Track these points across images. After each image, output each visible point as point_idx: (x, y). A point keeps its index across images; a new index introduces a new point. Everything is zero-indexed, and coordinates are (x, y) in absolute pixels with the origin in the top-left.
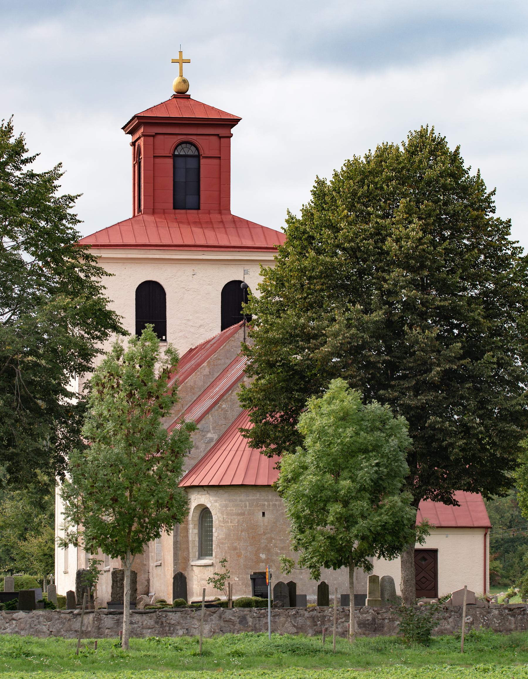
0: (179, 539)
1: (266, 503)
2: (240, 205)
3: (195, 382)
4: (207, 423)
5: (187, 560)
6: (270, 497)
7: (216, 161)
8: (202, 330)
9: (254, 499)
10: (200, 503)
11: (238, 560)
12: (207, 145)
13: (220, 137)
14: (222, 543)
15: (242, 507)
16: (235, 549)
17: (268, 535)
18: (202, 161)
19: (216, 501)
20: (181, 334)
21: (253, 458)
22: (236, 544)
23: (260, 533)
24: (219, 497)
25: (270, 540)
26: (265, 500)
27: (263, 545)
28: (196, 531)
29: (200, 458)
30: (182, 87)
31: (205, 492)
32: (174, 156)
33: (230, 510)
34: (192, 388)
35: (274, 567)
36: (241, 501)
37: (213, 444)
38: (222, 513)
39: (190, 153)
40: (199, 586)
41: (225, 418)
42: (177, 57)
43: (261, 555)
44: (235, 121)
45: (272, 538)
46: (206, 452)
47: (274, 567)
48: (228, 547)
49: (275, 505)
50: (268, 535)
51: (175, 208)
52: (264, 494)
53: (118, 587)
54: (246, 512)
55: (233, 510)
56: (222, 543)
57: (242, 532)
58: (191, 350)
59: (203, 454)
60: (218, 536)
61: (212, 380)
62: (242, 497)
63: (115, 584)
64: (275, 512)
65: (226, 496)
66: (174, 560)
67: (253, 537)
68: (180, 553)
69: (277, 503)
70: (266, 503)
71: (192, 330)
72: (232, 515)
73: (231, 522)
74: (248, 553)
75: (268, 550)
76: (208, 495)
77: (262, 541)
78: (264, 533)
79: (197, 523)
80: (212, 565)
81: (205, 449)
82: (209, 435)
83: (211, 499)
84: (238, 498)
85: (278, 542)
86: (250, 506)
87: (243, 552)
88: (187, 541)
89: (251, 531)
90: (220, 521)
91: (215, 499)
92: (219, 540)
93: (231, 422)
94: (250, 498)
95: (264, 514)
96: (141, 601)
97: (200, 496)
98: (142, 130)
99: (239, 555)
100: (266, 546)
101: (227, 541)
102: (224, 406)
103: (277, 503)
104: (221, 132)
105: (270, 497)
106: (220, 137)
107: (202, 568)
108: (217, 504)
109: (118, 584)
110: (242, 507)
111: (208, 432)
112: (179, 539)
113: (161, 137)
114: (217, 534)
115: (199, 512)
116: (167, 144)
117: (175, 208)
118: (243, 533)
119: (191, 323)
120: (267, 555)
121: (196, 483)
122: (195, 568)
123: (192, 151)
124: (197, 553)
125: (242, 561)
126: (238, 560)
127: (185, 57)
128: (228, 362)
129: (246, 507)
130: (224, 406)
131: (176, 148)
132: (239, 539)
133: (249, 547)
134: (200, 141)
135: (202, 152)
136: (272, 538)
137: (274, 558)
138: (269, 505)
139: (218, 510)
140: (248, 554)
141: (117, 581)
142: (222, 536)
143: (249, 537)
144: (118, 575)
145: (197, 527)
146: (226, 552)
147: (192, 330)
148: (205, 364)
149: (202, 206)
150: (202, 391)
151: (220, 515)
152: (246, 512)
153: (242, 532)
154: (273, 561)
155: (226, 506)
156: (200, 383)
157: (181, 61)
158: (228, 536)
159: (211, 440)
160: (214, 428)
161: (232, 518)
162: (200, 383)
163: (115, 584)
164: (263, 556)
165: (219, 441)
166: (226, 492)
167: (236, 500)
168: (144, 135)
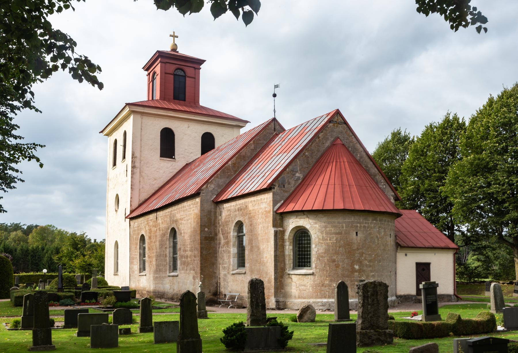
0: (278, 253)
1: (359, 225)
2: (204, 101)
3: (246, 153)
4: (296, 165)
5: (283, 269)
6: (361, 221)
7: (193, 80)
8: (192, 155)
9: (349, 222)
10: (298, 225)
11: (336, 270)
12: (189, 71)
13: (195, 68)
14: (322, 257)
15: (339, 228)
16: (334, 261)
17: (360, 251)
18: (187, 79)
19: (316, 223)
20: (182, 156)
21: (329, 191)
22: (335, 258)
23: (354, 248)
24: (318, 220)
25: (362, 254)
26: (358, 223)
27: (357, 259)
28: (291, 247)
29: (291, 192)
30: (175, 47)
31: (305, 216)
32: (174, 75)
33: (329, 230)
34: (244, 157)
35: (364, 276)
36: (339, 223)
37: (300, 181)
38: (322, 233)
39: (181, 74)
40: (298, 291)
41: (308, 163)
42: (172, 34)
43: (355, 266)
44: (202, 62)
45: (363, 253)
46: (295, 187)
47: (364, 276)
48: (328, 260)
49: (365, 227)
50: (360, 251)
51: (174, 99)
52: (357, 217)
53: (369, 304)
54: (343, 232)
55: (331, 230)
56: (322, 257)
57: (339, 247)
58: (187, 164)
59: (293, 189)
60: (318, 251)
61: (255, 153)
62: (342, 221)
63: (366, 301)
64: (365, 232)
65: (325, 219)
66: (275, 270)
67: (349, 252)
68: (279, 264)
69: (366, 225)
70: (359, 225)
71: (188, 154)
72: (331, 234)
73: (330, 240)
74: (345, 264)
75: (360, 262)
76: (307, 219)
77: (356, 255)
78: (358, 249)
79: (292, 241)
80: (313, 274)
81: (294, 185)
82: (297, 175)
83: (311, 221)
84: (336, 221)
85: (367, 256)
86: (346, 227)
87: (341, 264)
88: (284, 255)
89: (347, 247)
90: (320, 239)
91: (314, 221)
92: (319, 254)
93: (311, 166)
94: (347, 220)
95: (357, 233)
96: (307, 310)
97: (299, 220)
98: (160, 59)
99: (337, 266)
100: (359, 259)
101: (326, 255)
102: (307, 154)
103: (366, 225)
104: (196, 66)
105: (361, 221)
106: (195, 68)
107: (301, 276)
108: (317, 226)
109: (369, 300)
110: (339, 228)
111: (297, 172)
112: (278, 253)
113: (168, 64)
114: (316, 250)
115: (294, 232)
116: (171, 68)
117: (174, 99)
118: (341, 249)
119: (187, 151)
120: (360, 266)
121: (296, 209)
122: (293, 277)
123: (182, 73)
124: (292, 265)
125: (340, 271)
126: (336, 270)
127: (175, 35)
128: (265, 142)
129: (343, 227)
130: (307, 154)
131: (175, 71)
132: (337, 253)
133: (346, 260)
134: (187, 70)
135: (187, 74)
136: (363, 253)
137: (365, 268)
138: (361, 226)
139: (317, 230)
140: (345, 265)
141: (368, 297)
142: (321, 251)
143: (345, 252)
144: (369, 289)
145: (292, 244)
146: (325, 264)
147: (188, 154)
148: (252, 142)
149: (186, 100)
150: (250, 158)
151: (320, 234)
152: (343, 232)
153: (339, 247)
154: (364, 271)
155: (326, 227)
156: (249, 154)
157: (174, 36)
158: (327, 251)
159: (299, 178)
160: (300, 170)
161: (331, 236)
162: (249, 154)
163: (366, 301)
164: (357, 267)
165: (303, 180)
166: (325, 216)
167: (334, 222)
168: (160, 62)
